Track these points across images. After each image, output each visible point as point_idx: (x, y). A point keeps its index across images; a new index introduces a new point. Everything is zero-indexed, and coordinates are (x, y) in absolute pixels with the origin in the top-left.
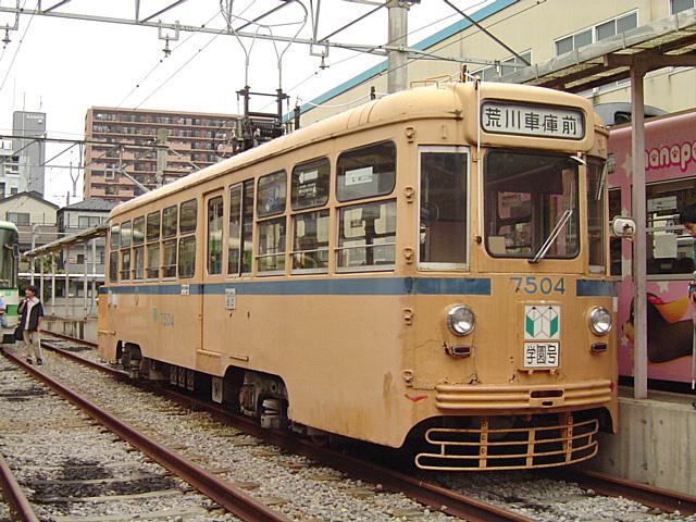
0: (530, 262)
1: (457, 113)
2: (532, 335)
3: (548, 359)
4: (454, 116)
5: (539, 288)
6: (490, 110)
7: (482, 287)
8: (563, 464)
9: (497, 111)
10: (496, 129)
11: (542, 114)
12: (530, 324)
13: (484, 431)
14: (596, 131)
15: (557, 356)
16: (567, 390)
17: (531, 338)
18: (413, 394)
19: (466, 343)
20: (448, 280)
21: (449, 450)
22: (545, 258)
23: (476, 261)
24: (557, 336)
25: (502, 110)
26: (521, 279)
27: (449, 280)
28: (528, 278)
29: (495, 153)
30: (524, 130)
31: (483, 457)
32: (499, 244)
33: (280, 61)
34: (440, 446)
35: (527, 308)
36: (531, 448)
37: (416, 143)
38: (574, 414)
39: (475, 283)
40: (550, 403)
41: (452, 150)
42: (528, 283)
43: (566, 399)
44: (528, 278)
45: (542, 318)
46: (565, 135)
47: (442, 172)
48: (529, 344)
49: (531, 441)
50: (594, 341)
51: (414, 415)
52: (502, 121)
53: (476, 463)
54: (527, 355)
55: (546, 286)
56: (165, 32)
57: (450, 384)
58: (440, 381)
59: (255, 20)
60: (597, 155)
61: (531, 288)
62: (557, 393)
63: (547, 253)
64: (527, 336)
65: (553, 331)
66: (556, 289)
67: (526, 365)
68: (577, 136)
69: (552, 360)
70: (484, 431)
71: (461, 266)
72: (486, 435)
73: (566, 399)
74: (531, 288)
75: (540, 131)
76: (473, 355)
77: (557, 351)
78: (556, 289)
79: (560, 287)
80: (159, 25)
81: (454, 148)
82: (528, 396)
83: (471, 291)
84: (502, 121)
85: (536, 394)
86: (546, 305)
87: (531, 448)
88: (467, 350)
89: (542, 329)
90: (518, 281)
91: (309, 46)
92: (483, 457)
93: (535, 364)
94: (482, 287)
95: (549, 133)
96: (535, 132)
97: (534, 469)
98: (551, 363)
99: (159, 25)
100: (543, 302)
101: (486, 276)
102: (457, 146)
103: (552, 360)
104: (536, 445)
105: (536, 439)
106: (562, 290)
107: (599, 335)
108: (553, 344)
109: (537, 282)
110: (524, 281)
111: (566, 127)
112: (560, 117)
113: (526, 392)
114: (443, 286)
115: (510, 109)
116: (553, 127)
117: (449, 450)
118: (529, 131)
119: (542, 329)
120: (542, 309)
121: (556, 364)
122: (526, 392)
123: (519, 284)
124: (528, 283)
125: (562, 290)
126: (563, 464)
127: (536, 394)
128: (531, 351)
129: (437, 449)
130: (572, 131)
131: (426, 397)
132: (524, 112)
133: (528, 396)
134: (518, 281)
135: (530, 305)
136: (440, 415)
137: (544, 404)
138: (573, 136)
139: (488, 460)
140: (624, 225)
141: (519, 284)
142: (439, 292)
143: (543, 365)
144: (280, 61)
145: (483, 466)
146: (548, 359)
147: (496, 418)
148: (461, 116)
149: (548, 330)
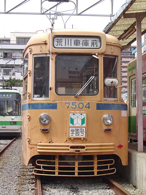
0: (75, 97)
1: (46, 41)
2: (73, 125)
3: (80, 134)
4: (44, 43)
5: (77, 107)
6: (58, 40)
7: (54, 106)
8: (93, 176)
9: (61, 40)
10: (60, 46)
11: (81, 40)
12: (72, 121)
13: (57, 161)
14: (107, 44)
15: (84, 133)
16: (87, 146)
17: (73, 126)
18: (31, 146)
19: (47, 127)
20: (42, 104)
21: (107, 167)
22: (80, 95)
23: (52, 97)
24: (84, 125)
25: (64, 40)
26: (69, 103)
27: (42, 104)
28: (73, 103)
29: (59, 55)
30: (73, 46)
31: (57, 171)
32: (62, 90)
33: (65, 25)
34: (41, 166)
35: (71, 115)
36: (76, 169)
37: (32, 54)
38: (98, 156)
39: (51, 105)
40: (79, 151)
41: (45, 56)
42: (73, 105)
43: (86, 150)
44: (73, 103)
45: (78, 119)
46: (92, 47)
47: (41, 63)
48: (72, 128)
49: (96, 171)
50: (105, 128)
51: (30, 154)
52: (63, 43)
53: (54, 173)
54: (70, 132)
55: (81, 106)
56: (52, 16)
57: (42, 143)
58: (39, 142)
59: (49, 9)
60: (111, 54)
61: (74, 107)
62: (83, 147)
63: (81, 93)
64: (71, 125)
65: (83, 123)
66: (85, 107)
67: (70, 136)
68: (98, 47)
69: (82, 134)
70: (57, 161)
71: (47, 99)
72: (57, 162)
73: (86, 150)
74: (74, 107)
75: (81, 46)
76: (50, 132)
77: (84, 131)
78: (85, 107)
79: (88, 106)
80: (50, 14)
81: (45, 55)
82: (69, 148)
83: (50, 108)
84: (63, 43)
85: (72, 147)
86: (79, 113)
87: (76, 169)
88: (110, 130)
89: (78, 122)
90: (68, 104)
91: (110, 17)
92: (57, 171)
93: (74, 136)
94: (54, 106)
95: (85, 47)
96: (78, 47)
97: (58, 176)
98: (82, 135)
99: (50, 14)
100: (78, 112)
101: (55, 102)
102: (46, 54)
103: (82, 134)
104: (59, 167)
105: (78, 165)
106: (89, 107)
107: (108, 125)
108: (82, 128)
109: (77, 104)
110: (71, 104)
111: (93, 44)
112: (90, 41)
113: (68, 146)
114: (40, 107)
115: (67, 39)
116: (87, 44)
117: (107, 167)
118: (76, 47)
119: (78, 122)
120: (78, 115)
121: (84, 136)
122: (68, 146)
123: (69, 105)
124: (73, 105)
125: (89, 107)
126: (93, 176)
127: (72, 147)
128: (73, 131)
129: (39, 167)
130: (95, 46)
131: (34, 147)
132: (73, 40)
133: (69, 148)
134: (68, 104)
135: (72, 113)
136: (39, 154)
137: (76, 151)
138: (96, 47)
139: (59, 172)
140: (111, 81)
141: (69, 105)
142: (38, 109)
143: (78, 136)
144: (65, 25)
145: (96, 174)
146: (80, 134)
147: (62, 157)
148: (47, 43)
149: (80, 122)
